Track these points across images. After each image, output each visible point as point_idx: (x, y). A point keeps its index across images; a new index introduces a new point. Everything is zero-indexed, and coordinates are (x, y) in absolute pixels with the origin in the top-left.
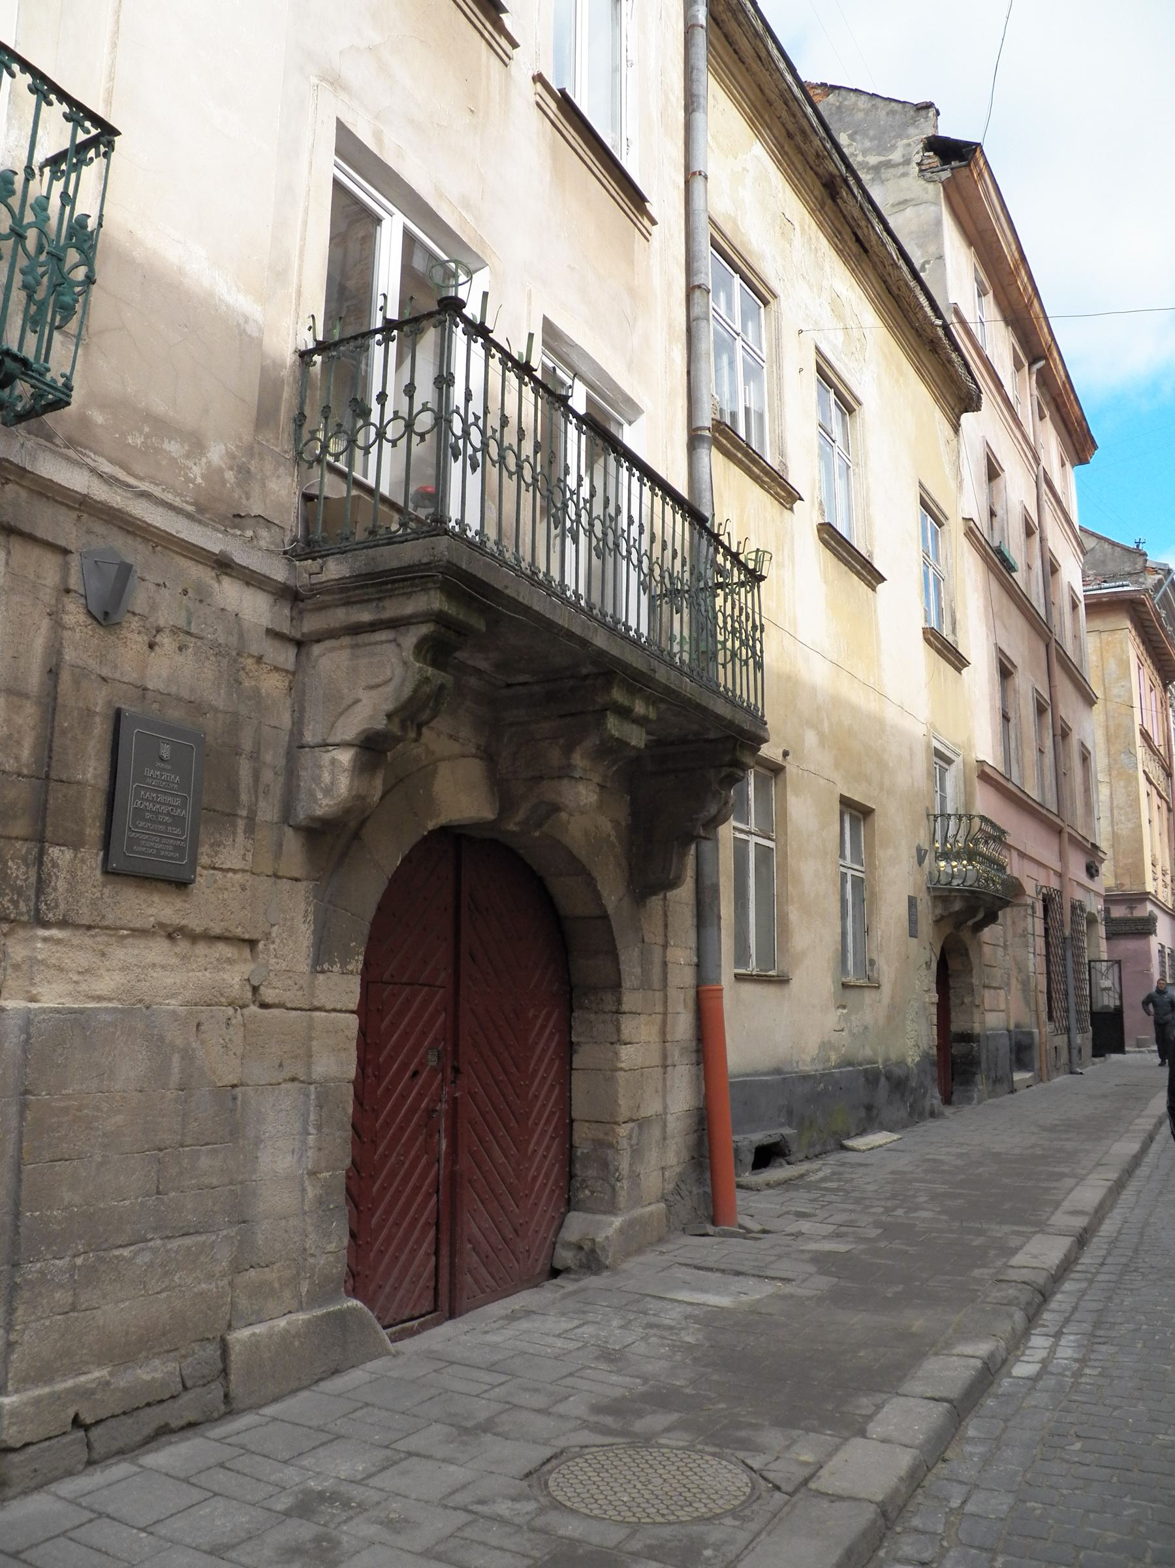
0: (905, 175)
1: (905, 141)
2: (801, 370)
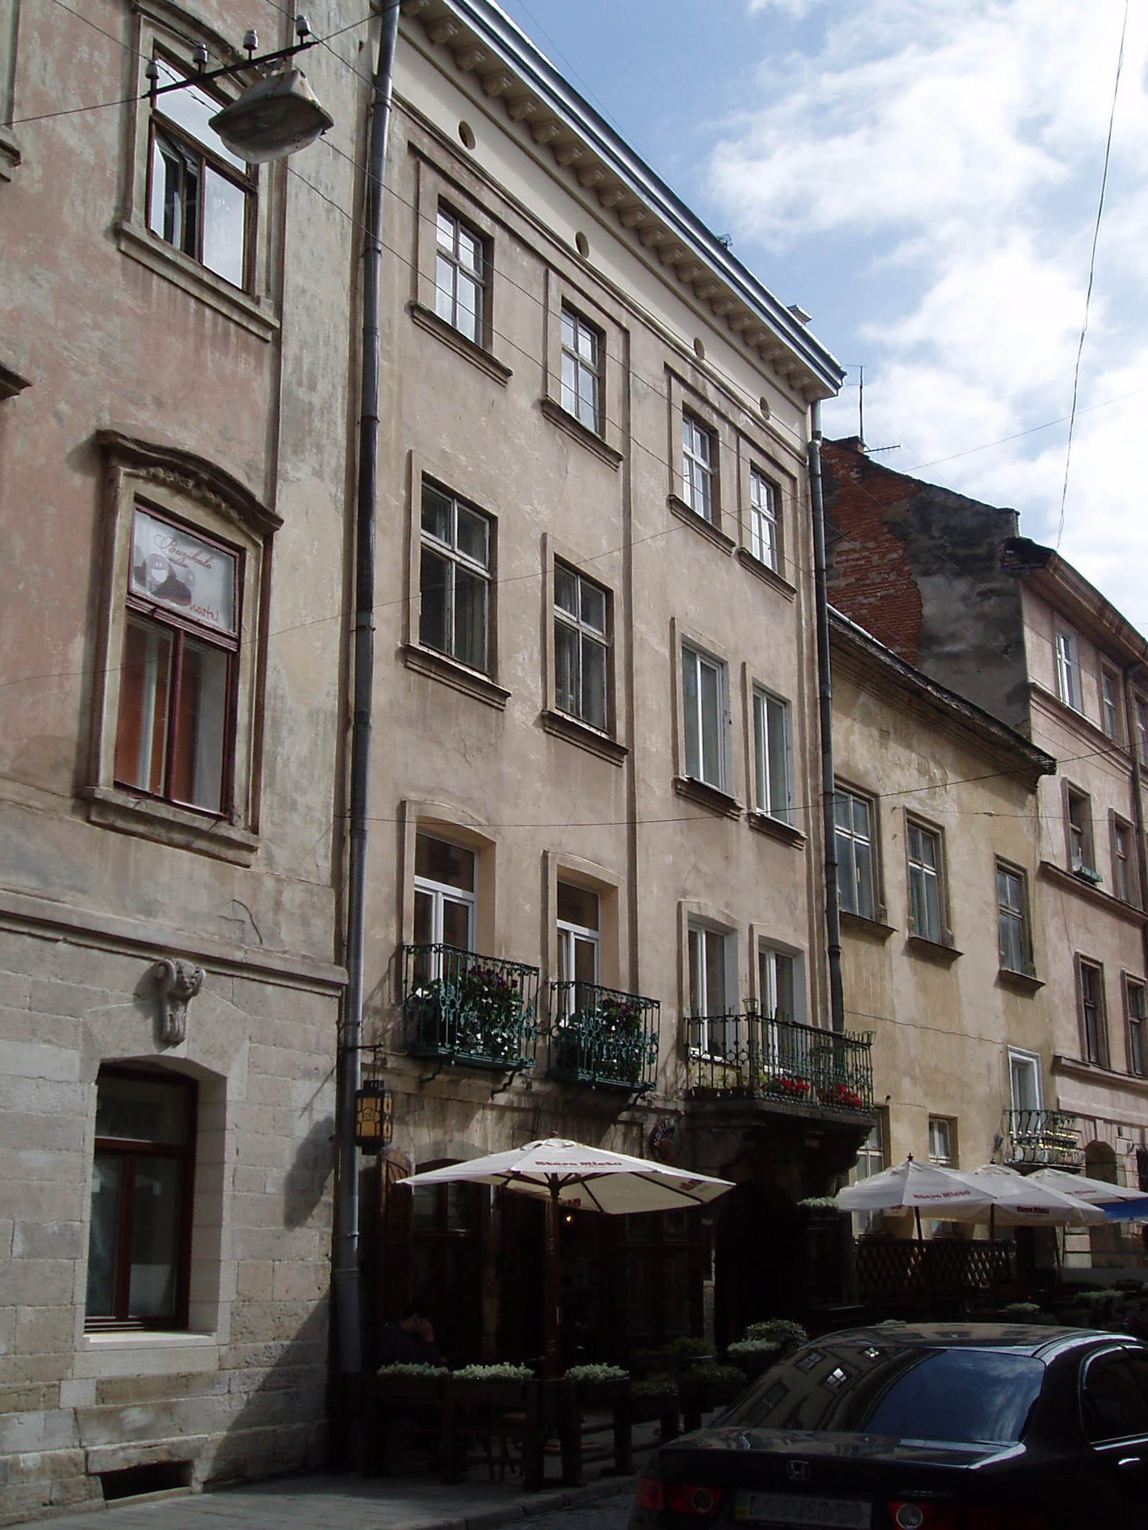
2: (895, 836)
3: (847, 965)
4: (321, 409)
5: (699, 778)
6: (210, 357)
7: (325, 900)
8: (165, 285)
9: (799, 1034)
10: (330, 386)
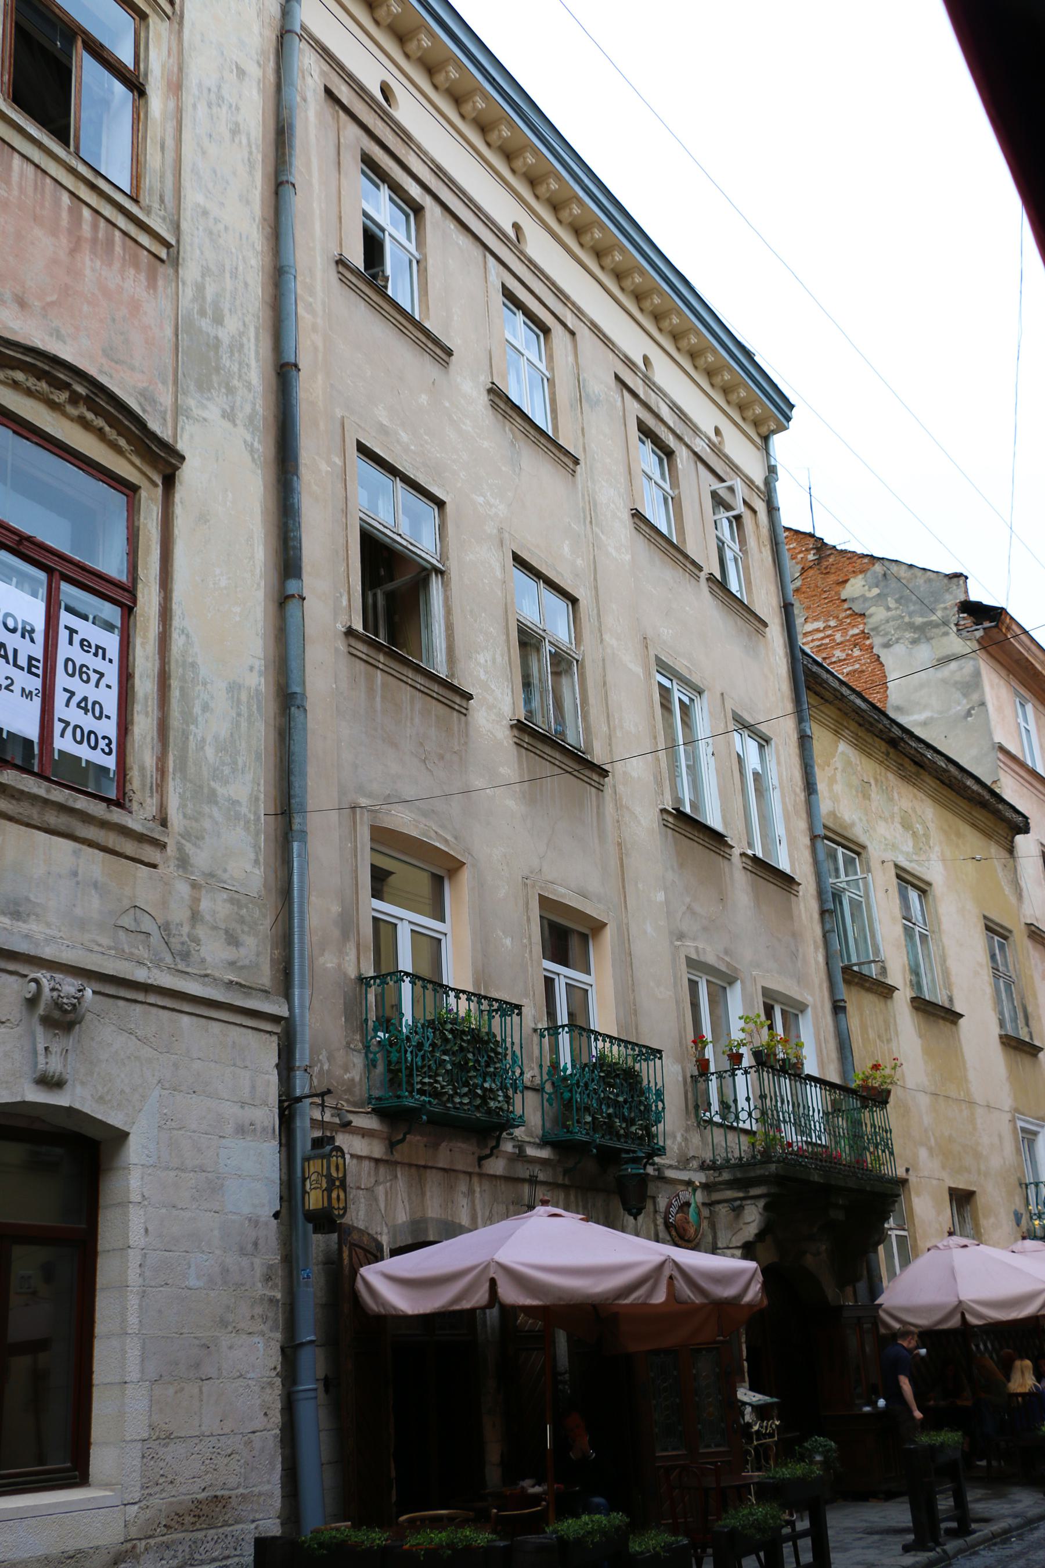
0: (946, 634)
1: (942, 606)
2: (887, 891)
3: (854, 1021)
4: (231, 347)
5: (685, 808)
6: (89, 264)
7: (257, 913)
8: (30, 169)
9: (813, 1088)
10: (240, 323)
